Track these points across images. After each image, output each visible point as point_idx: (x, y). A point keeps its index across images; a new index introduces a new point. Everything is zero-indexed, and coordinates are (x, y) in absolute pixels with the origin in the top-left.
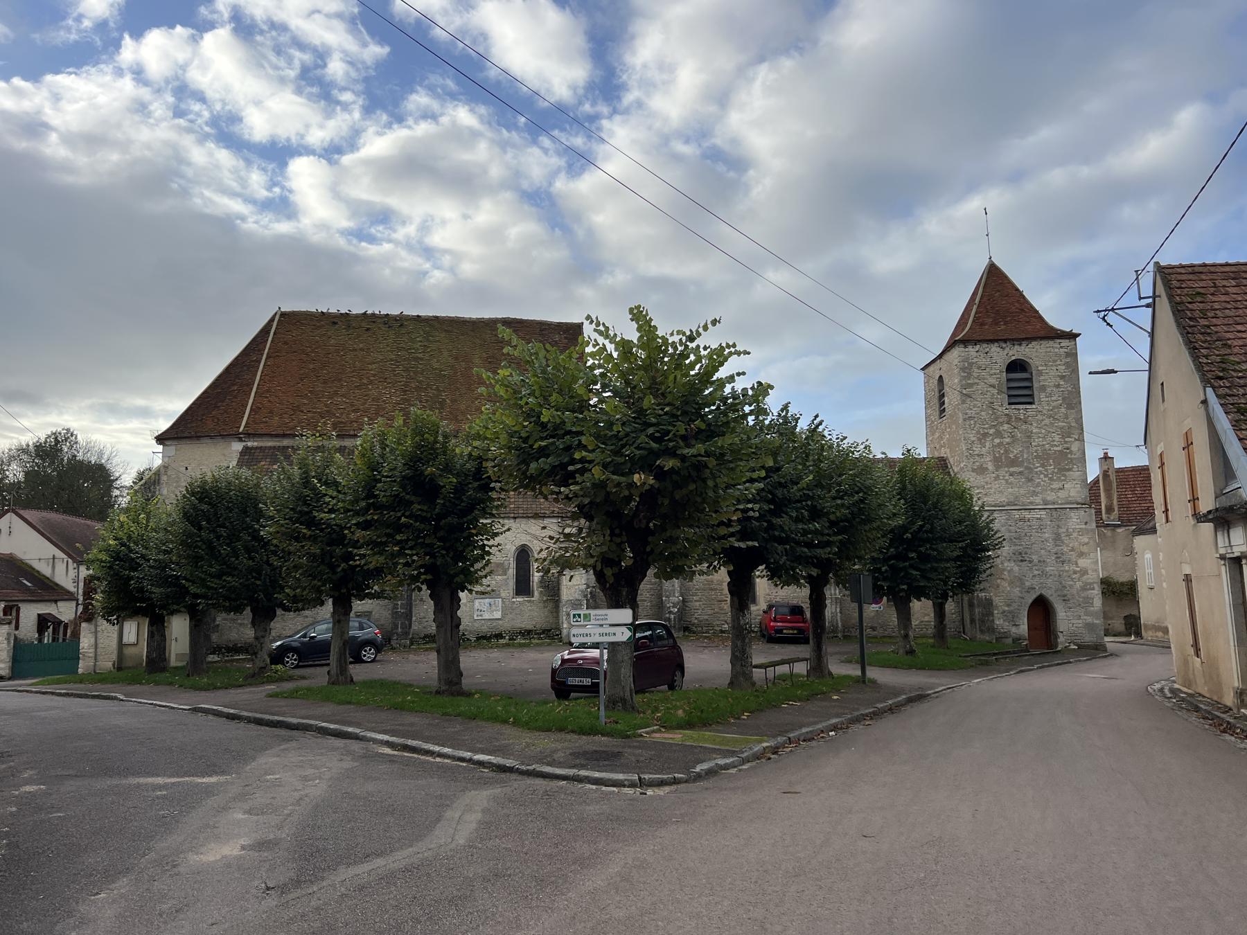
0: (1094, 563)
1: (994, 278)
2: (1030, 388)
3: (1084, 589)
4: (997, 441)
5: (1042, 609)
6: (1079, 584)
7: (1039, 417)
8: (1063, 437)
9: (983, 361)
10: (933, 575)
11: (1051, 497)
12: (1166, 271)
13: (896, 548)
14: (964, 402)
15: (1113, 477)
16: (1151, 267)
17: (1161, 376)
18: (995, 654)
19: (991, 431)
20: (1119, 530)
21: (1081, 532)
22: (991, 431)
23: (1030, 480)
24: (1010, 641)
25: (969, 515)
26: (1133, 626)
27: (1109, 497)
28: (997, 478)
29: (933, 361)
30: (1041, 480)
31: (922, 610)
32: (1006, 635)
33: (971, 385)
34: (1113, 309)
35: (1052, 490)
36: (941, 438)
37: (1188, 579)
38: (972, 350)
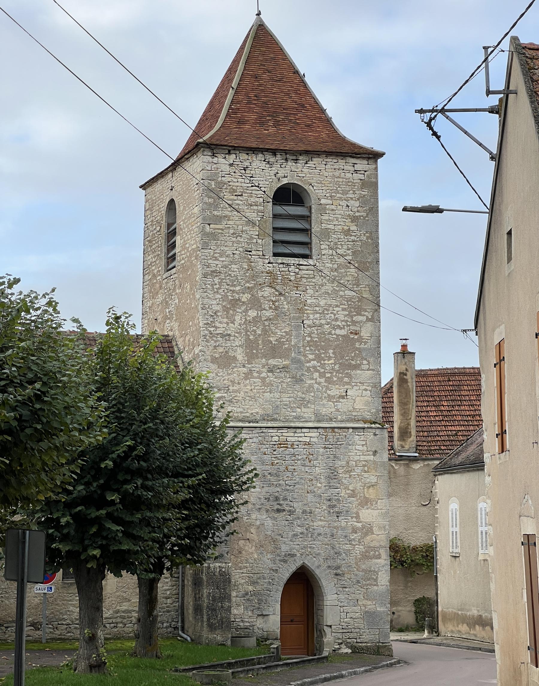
0: (379, 519)
1: (262, 44)
2: (306, 231)
3: (365, 556)
4: (252, 313)
5: (302, 587)
6: (359, 549)
7: (318, 280)
8: (350, 315)
9: (239, 182)
10: (144, 533)
11: (328, 409)
12: (529, 53)
13: (88, 484)
14: (205, 246)
15: (412, 384)
16: (506, 45)
17: (509, 219)
18: (230, 665)
19: (245, 297)
20: (416, 466)
21: (367, 467)
22: (245, 297)
23: (298, 380)
24: (252, 642)
25: (205, 433)
26: (426, 616)
27: (405, 414)
28: (248, 375)
29: (162, 175)
30: (314, 380)
31: (120, 591)
32: (247, 632)
33: (218, 219)
34: (443, 111)
35: (330, 398)
36: (166, 303)
37: (529, 542)
38: (223, 162)
